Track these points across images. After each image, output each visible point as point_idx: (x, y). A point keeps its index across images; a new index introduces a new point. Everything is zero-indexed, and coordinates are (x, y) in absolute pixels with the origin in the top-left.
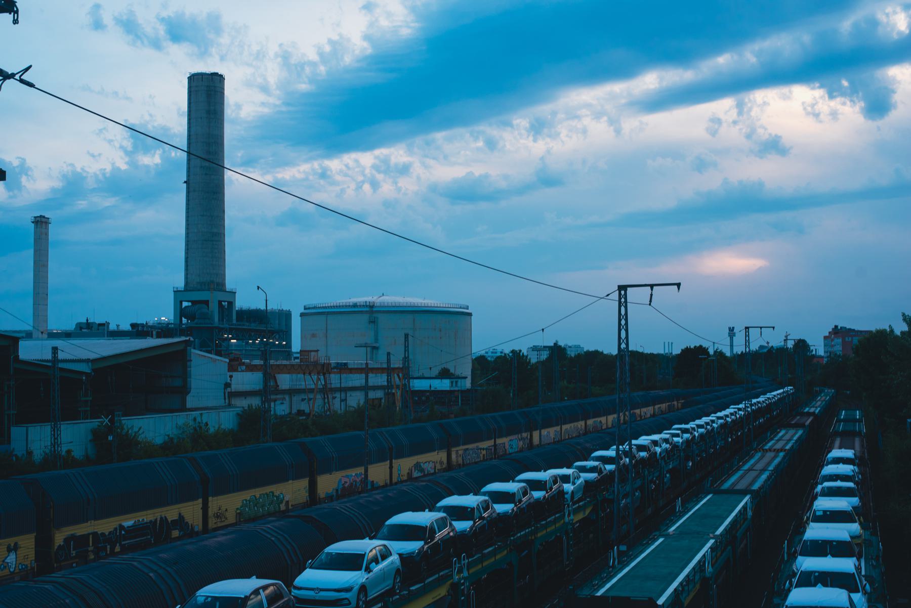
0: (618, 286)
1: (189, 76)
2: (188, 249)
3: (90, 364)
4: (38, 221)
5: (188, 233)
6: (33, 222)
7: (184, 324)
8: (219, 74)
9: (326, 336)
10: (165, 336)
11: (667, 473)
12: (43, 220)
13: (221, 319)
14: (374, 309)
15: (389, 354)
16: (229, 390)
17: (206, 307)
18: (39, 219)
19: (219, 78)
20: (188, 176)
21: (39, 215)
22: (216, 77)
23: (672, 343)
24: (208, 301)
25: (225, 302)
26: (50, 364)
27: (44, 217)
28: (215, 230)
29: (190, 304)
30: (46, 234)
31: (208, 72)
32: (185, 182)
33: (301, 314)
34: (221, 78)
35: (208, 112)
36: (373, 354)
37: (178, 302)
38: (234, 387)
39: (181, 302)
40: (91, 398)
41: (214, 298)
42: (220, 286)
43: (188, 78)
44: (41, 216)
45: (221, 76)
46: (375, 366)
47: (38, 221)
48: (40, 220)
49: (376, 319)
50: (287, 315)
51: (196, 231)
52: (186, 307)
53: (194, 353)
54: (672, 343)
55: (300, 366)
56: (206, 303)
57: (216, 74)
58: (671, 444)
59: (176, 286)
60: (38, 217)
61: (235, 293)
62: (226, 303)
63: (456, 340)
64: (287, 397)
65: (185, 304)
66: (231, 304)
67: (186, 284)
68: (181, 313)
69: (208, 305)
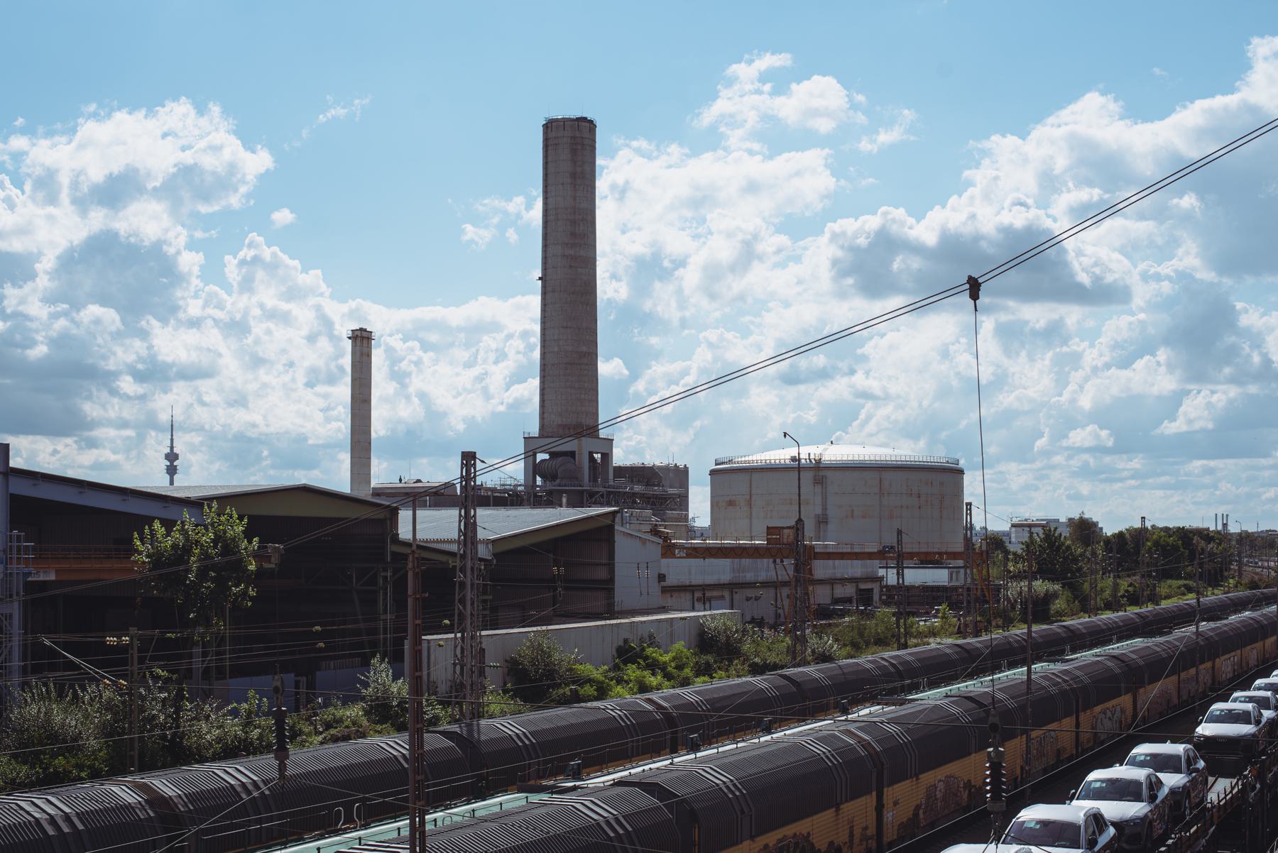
0: (463, 452)
1: (545, 122)
2: (544, 377)
3: (490, 546)
4: (357, 336)
5: (544, 353)
6: (349, 338)
7: (538, 486)
8: (589, 119)
9: (750, 505)
10: (581, 504)
11: (198, 641)
12: (365, 334)
13: (593, 479)
14: (821, 466)
15: (899, 532)
16: (663, 584)
17: (572, 460)
18: (359, 333)
19: (588, 125)
20: (545, 269)
21: (358, 328)
22: (584, 124)
23: (1227, 515)
24: (574, 452)
25: (597, 453)
26: (454, 548)
27: (365, 330)
28: (584, 349)
29: (546, 456)
30: (368, 356)
31: (572, 117)
32: (540, 279)
33: (710, 472)
34: (592, 125)
35: (574, 175)
36: (819, 531)
37: (530, 454)
38: (671, 580)
39: (534, 455)
40: (491, 597)
41: (582, 446)
42: (593, 430)
43: (543, 126)
44: (361, 329)
45: (591, 122)
46: (845, 551)
47: (357, 336)
48: (359, 335)
49: (824, 480)
50: (681, 475)
51: (556, 349)
52: (543, 461)
53: (618, 530)
54: (1227, 515)
55: (767, 549)
56: (572, 454)
57: (584, 119)
58: (795, 644)
59: (527, 430)
60: (357, 330)
61: (613, 440)
62: (599, 455)
63: (941, 512)
64: (726, 594)
65: (541, 457)
66: (607, 456)
67: (542, 427)
68: (534, 469)
69: (574, 458)
